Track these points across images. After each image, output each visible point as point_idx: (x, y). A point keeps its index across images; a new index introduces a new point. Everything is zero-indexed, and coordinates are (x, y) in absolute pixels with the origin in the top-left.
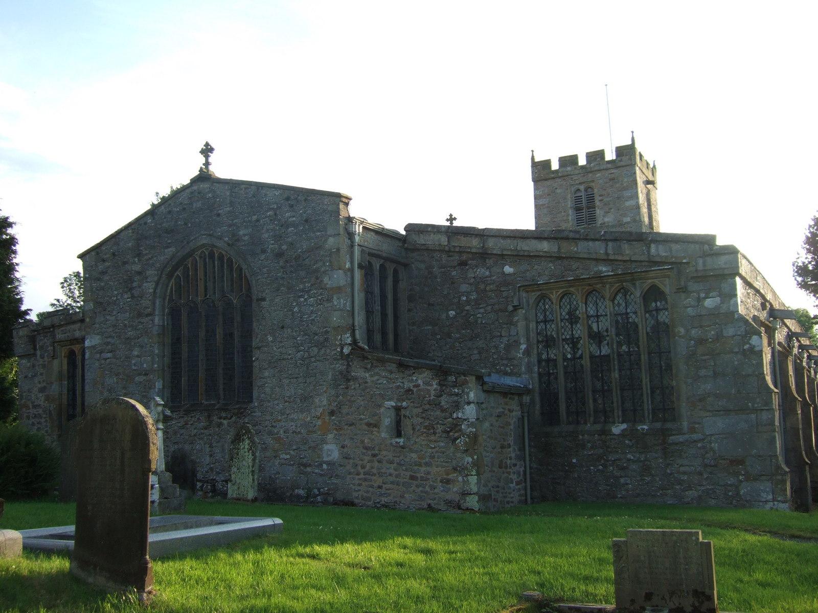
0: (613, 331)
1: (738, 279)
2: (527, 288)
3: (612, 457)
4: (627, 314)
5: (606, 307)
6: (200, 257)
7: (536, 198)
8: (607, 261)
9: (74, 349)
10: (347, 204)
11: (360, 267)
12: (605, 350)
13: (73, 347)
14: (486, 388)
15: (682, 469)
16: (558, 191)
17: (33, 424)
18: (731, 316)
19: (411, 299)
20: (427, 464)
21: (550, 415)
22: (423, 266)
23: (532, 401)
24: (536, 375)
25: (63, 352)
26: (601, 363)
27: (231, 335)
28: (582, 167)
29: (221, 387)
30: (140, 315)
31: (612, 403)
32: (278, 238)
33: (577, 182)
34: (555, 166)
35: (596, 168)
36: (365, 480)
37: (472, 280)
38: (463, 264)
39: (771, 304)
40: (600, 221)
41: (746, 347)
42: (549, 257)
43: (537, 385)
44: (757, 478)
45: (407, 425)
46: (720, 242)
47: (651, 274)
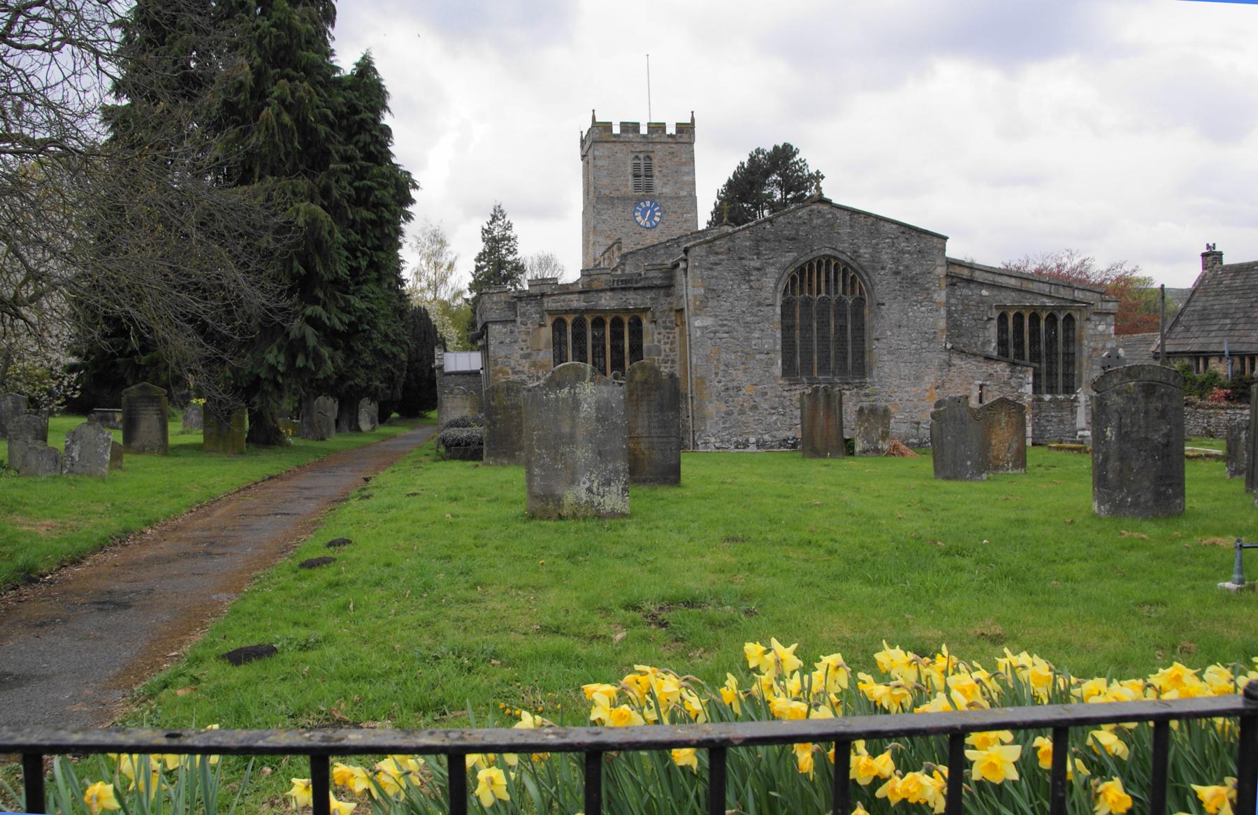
8: (1050, 297)
16: (619, 155)
25: (549, 321)
30: (759, 304)
32: (897, 261)
34: (616, 130)
40: (657, 192)
42: (1014, 289)
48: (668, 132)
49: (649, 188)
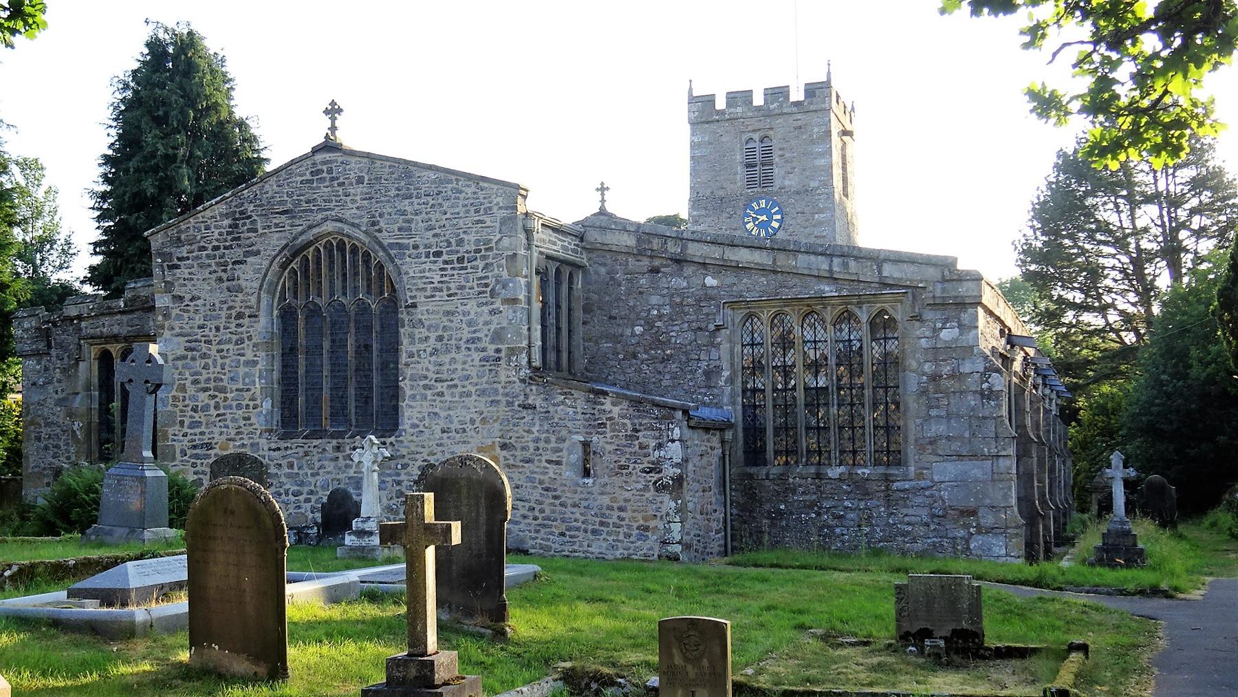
0: (832, 361)
1: (980, 311)
2: (733, 305)
3: (826, 504)
4: (850, 341)
5: (827, 334)
6: (325, 247)
7: (694, 146)
8: (832, 278)
9: (112, 350)
10: (525, 197)
11: (538, 273)
12: (822, 383)
13: (108, 347)
14: (692, 423)
15: (907, 519)
17: (46, 448)
18: (969, 350)
19: (587, 309)
20: (621, 509)
21: (755, 455)
22: (603, 270)
23: (735, 436)
24: (740, 407)
25: (92, 352)
26: (816, 397)
27: (368, 347)
28: (759, 108)
29: (353, 411)
31: (829, 442)
33: (750, 128)
34: (721, 104)
35: (777, 111)
36: (545, 526)
37: (665, 291)
38: (655, 271)
39: (1010, 330)
40: (777, 183)
41: (985, 386)
42: (763, 270)
43: (740, 419)
44: (990, 530)
45: (598, 466)
46: (960, 266)
47: (883, 298)
48: (793, 98)
49: (768, 180)
